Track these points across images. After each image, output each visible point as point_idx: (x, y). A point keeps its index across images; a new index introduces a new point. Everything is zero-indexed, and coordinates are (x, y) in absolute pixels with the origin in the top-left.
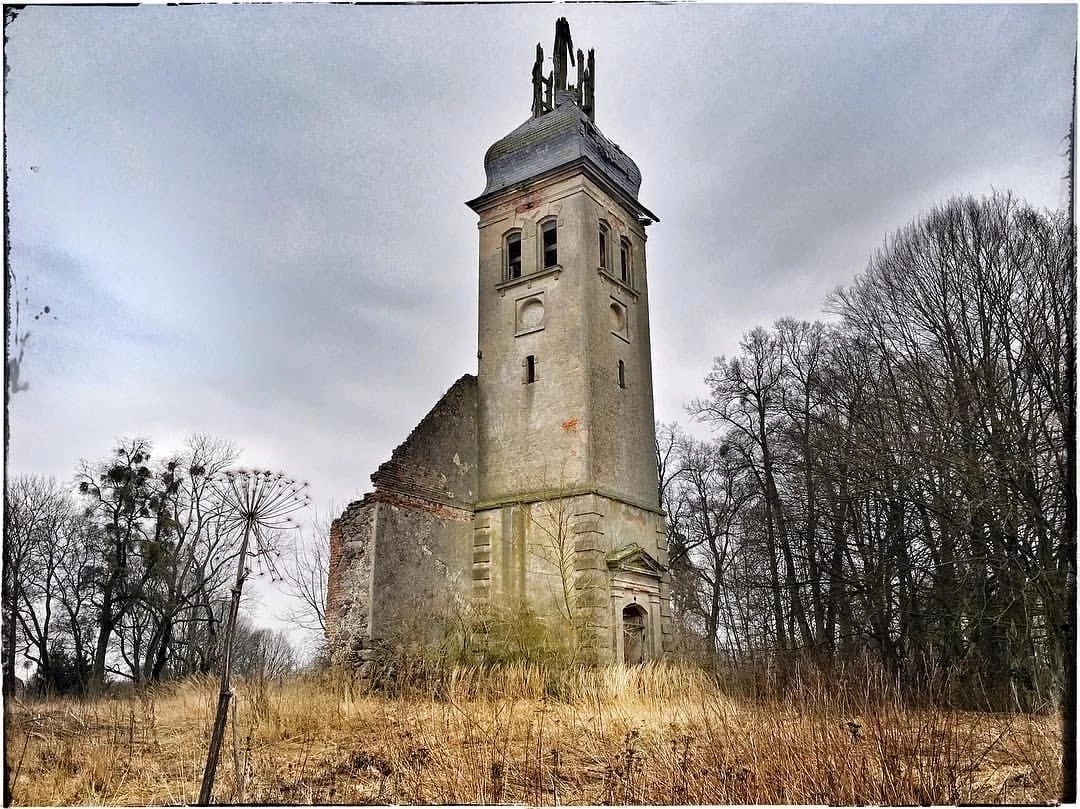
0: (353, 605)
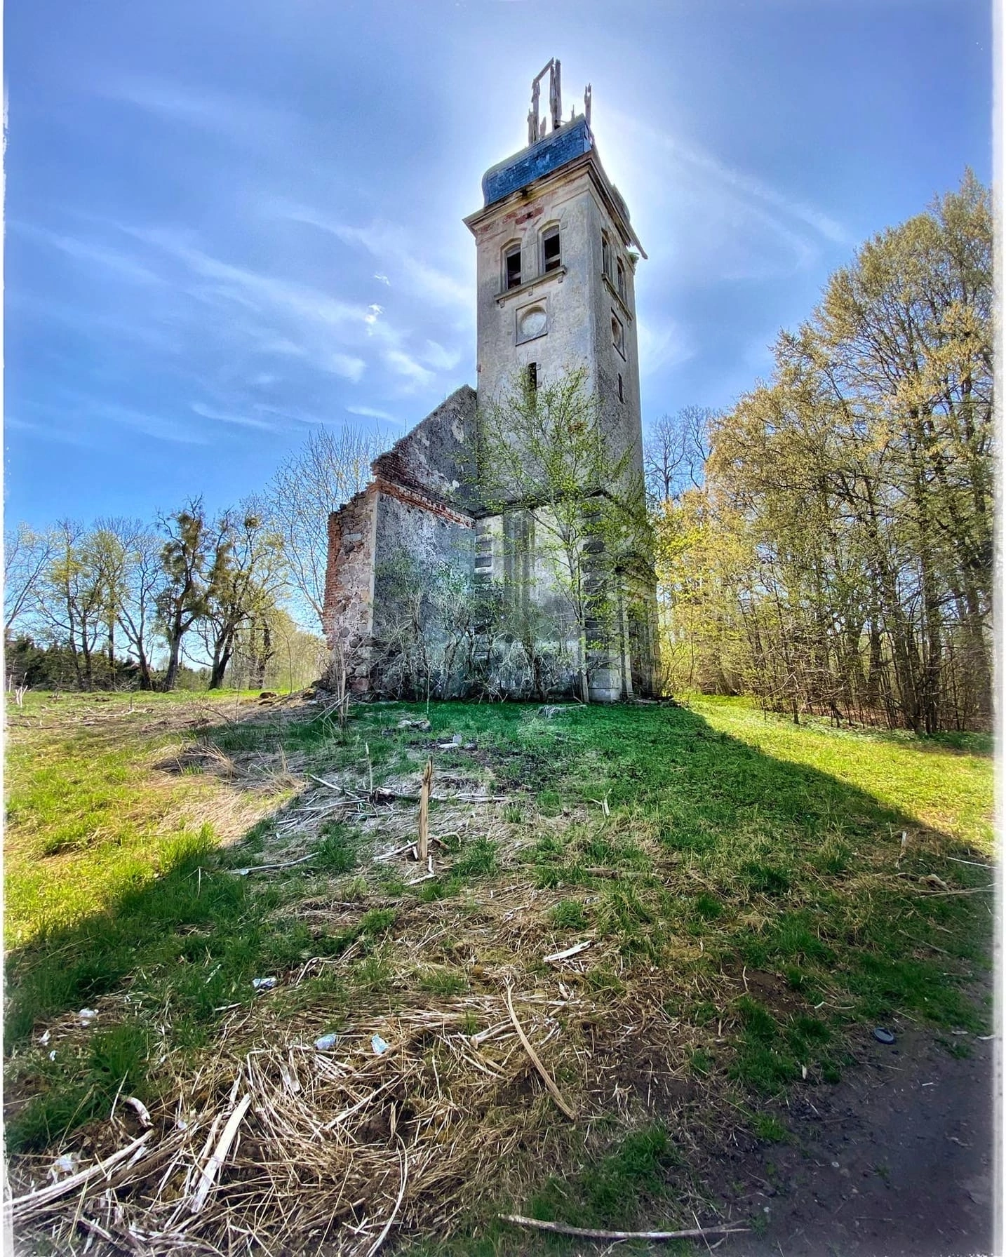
0: (352, 601)
